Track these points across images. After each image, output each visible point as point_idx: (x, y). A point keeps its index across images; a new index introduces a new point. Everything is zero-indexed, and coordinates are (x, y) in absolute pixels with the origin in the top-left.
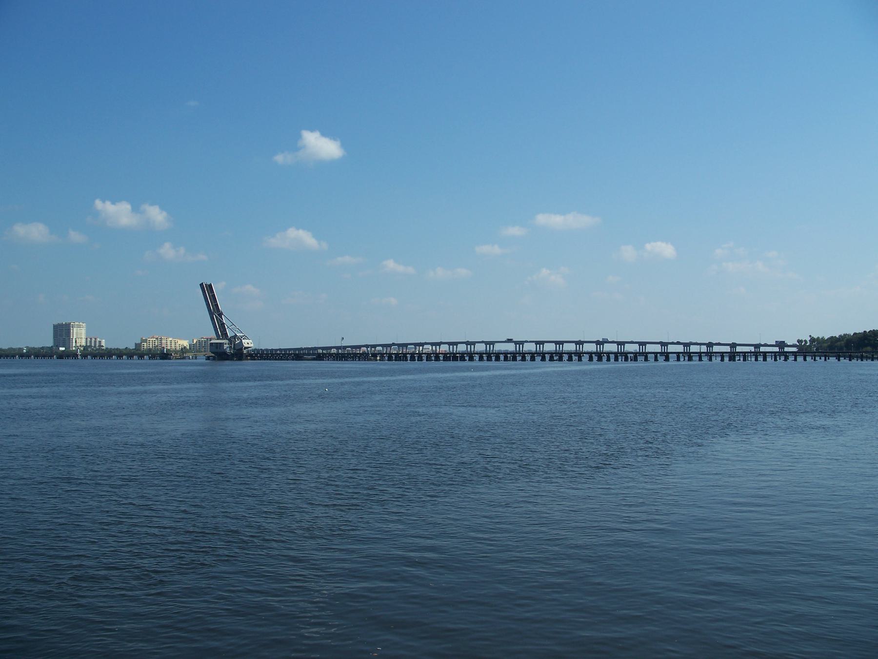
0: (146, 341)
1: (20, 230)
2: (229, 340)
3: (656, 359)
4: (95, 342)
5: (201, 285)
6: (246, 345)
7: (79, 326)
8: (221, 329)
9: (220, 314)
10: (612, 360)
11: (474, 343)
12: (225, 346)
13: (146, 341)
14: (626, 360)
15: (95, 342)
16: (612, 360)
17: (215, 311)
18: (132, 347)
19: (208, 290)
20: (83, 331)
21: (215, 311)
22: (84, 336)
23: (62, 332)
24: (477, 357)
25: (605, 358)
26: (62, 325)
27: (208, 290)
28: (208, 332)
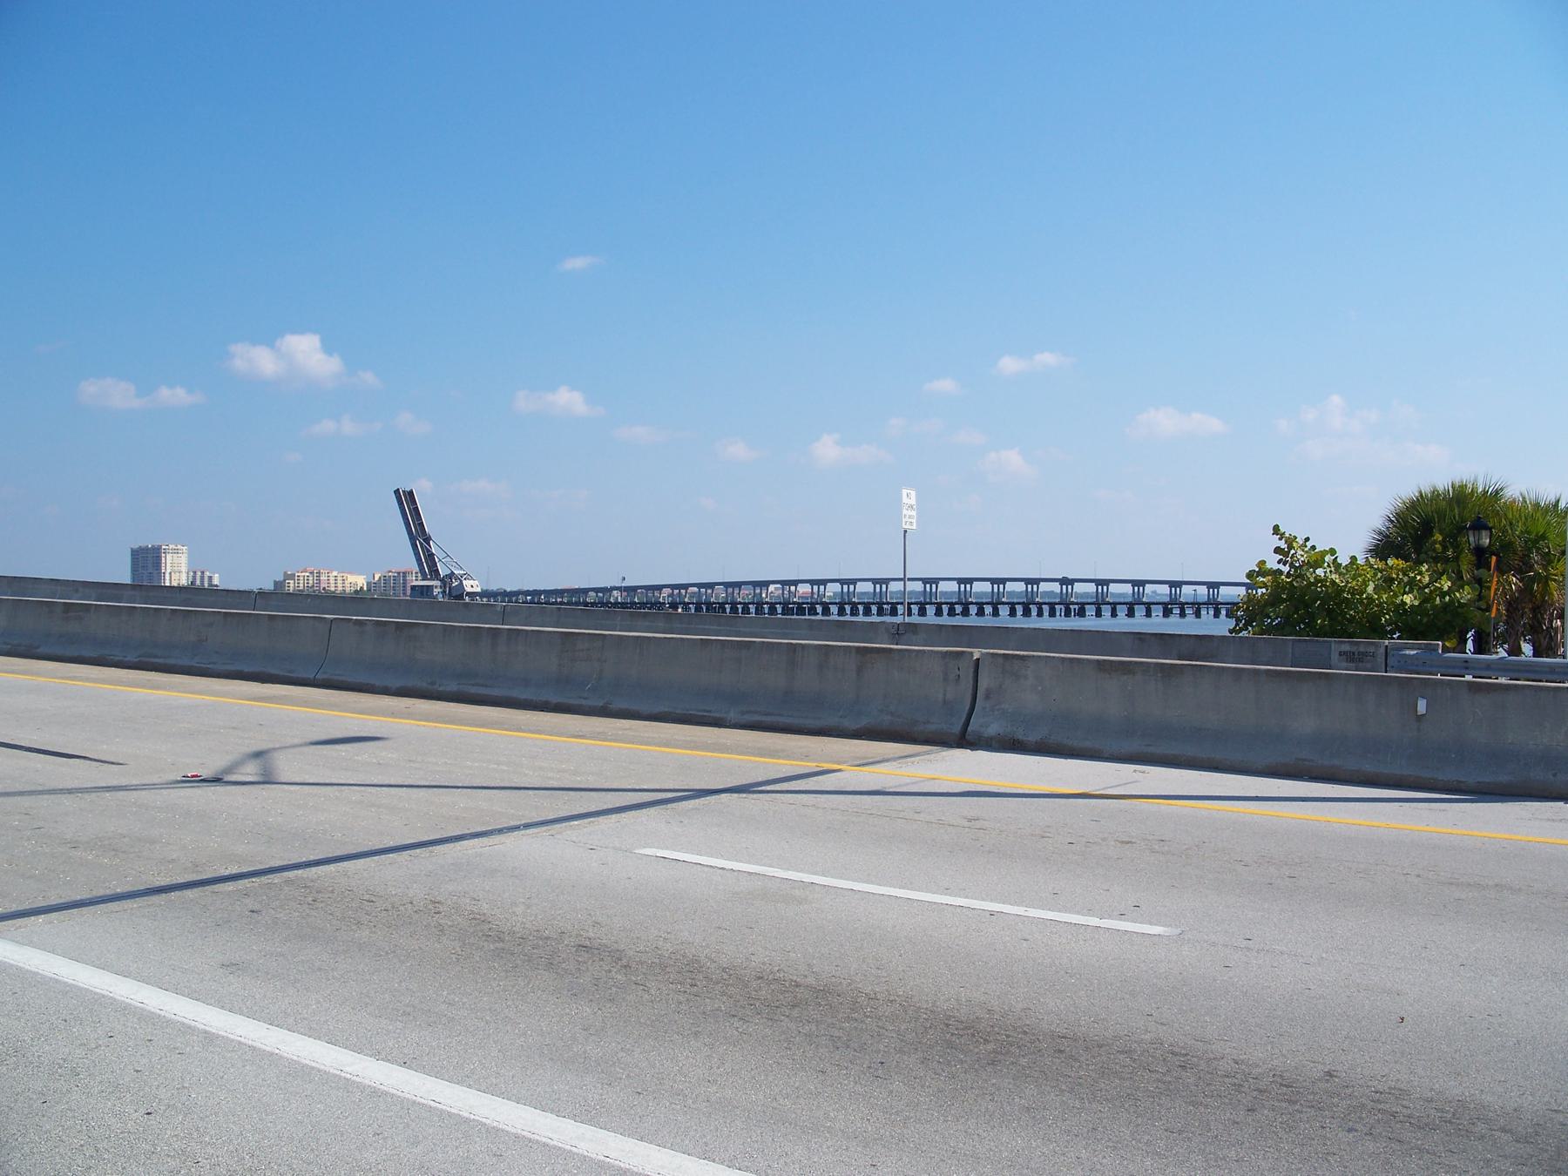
0: (292, 577)
1: (90, 389)
2: (442, 580)
3: (1198, 615)
4: (202, 578)
5: (397, 492)
6: (469, 589)
7: (176, 551)
8: (428, 563)
9: (428, 539)
10: (1046, 613)
11: (854, 582)
12: (436, 591)
13: (292, 577)
14: (1068, 614)
15: (202, 578)
16: (1046, 613)
17: (418, 535)
18: (269, 586)
19: (407, 501)
20: (183, 561)
21: (418, 535)
22: (184, 569)
23: (147, 559)
24: (973, 610)
25: (1034, 611)
26: (147, 549)
27: (407, 501)
28: (404, 560)
